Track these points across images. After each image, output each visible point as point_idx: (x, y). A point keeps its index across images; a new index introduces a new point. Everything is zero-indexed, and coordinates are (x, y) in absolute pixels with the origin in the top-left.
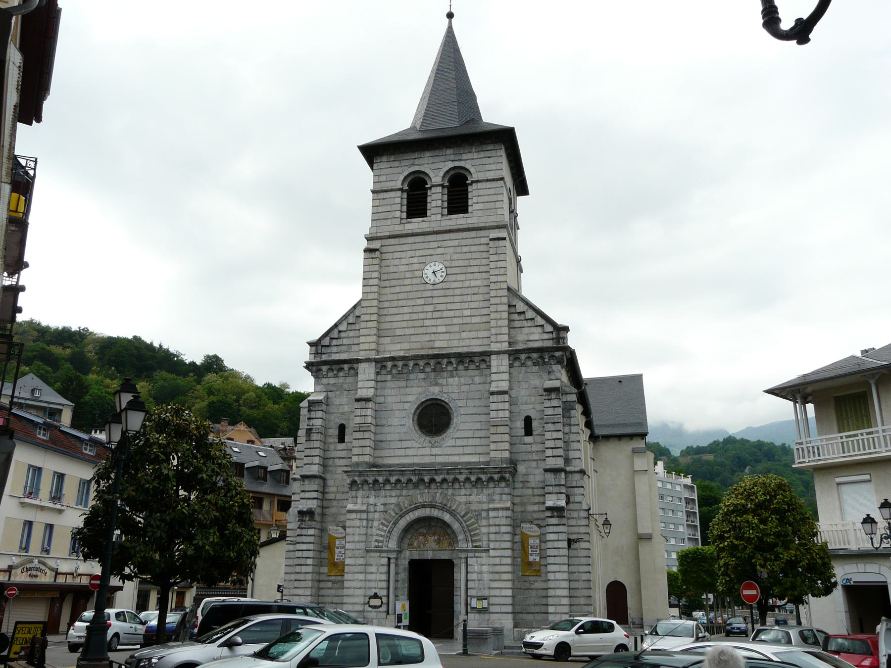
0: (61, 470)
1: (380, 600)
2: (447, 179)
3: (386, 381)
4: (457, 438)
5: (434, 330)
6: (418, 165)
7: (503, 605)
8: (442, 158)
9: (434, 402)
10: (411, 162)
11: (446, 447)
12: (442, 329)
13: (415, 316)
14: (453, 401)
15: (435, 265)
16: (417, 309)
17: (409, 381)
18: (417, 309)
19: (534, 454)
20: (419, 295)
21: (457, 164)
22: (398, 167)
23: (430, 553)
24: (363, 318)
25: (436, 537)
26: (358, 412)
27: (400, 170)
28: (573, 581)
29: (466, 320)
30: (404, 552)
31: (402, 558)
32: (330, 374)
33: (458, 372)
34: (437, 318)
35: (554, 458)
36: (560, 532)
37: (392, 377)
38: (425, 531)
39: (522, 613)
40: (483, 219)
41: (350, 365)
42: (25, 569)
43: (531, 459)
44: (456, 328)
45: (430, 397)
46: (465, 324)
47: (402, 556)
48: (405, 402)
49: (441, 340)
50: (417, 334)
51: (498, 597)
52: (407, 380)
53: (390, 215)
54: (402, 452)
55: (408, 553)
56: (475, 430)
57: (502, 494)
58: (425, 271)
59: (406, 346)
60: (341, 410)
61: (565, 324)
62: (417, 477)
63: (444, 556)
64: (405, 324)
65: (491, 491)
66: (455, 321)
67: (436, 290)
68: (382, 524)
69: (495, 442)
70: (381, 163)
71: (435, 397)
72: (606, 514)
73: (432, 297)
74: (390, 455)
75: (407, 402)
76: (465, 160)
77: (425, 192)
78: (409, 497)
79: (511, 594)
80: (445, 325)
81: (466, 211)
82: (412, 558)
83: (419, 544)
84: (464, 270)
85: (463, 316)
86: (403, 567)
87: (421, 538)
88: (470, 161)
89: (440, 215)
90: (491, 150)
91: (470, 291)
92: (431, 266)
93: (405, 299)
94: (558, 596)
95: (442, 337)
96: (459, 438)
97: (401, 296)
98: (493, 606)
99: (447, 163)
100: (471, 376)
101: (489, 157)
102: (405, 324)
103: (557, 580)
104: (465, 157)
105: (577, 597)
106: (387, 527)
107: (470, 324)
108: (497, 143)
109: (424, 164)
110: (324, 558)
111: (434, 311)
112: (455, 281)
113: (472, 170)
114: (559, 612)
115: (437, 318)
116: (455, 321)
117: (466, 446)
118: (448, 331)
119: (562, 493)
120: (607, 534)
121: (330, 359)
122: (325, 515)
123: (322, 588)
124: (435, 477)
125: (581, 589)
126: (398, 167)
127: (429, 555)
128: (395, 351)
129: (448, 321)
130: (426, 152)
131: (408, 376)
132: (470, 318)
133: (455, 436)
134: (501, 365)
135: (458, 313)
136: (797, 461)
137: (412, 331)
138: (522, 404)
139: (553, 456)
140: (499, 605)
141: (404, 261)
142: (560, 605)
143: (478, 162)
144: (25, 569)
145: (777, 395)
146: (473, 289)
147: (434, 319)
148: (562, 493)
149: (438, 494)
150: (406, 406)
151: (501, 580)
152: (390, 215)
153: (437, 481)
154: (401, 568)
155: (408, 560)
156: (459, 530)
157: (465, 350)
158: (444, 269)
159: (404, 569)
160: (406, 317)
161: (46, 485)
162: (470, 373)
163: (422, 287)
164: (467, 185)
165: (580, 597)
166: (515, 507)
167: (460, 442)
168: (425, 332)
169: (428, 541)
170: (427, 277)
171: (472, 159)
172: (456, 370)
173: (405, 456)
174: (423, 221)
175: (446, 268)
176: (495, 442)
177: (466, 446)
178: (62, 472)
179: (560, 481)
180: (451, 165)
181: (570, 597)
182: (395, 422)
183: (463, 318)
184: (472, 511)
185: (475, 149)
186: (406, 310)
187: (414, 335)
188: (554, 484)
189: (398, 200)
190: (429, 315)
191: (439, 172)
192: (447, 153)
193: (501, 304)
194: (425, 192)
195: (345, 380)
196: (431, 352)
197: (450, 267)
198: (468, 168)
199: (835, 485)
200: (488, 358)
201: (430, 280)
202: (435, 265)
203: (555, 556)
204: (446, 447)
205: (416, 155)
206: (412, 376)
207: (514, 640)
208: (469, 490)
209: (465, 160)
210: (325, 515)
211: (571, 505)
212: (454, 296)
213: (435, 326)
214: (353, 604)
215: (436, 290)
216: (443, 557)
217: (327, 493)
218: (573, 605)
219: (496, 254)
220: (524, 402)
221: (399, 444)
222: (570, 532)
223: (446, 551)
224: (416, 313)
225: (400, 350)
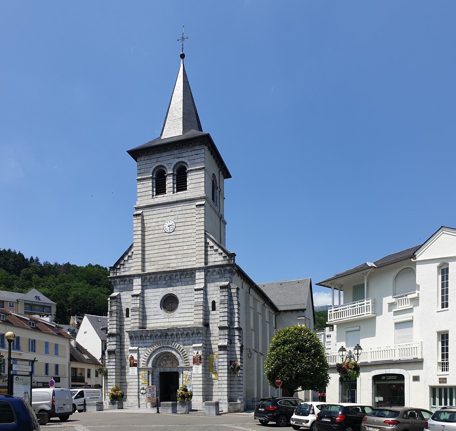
1: (145, 391)
2: (155, 174)
3: (147, 285)
4: (180, 313)
5: (170, 257)
7: (198, 392)
9: (171, 295)
10: (156, 160)
13: (160, 251)
14: (179, 294)
16: (161, 247)
17: (158, 285)
18: (161, 247)
20: (162, 239)
21: (180, 160)
23: (168, 369)
24: (135, 253)
26: (133, 302)
27: (148, 166)
29: (185, 252)
30: (157, 368)
31: (156, 371)
32: (121, 283)
33: (181, 279)
34: (171, 251)
35: (223, 322)
36: (224, 358)
37: (150, 283)
39: (209, 395)
42: (4, 380)
43: (215, 322)
44: (180, 256)
45: (168, 293)
46: (185, 254)
47: (156, 370)
49: (173, 263)
50: (162, 260)
51: (197, 388)
52: (157, 284)
54: (155, 321)
55: (158, 369)
56: (189, 309)
58: (165, 226)
60: (127, 301)
61: (68, 262)
62: (175, 332)
64: (155, 255)
65: (194, 338)
66: (180, 252)
68: (145, 356)
69: (196, 314)
71: (170, 293)
72: (250, 349)
73: (168, 240)
74: (150, 323)
76: (184, 157)
77: (165, 178)
78: (157, 343)
80: (175, 255)
81: (186, 189)
82: (160, 371)
83: (163, 364)
85: (184, 250)
86: (157, 375)
87: (164, 362)
88: (187, 157)
89: (172, 192)
91: (187, 236)
92: (167, 223)
95: (173, 261)
96: (182, 313)
97: (153, 240)
99: (175, 159)
100: (187, 281)
101: (197, 154)
102: (155, 255)
103: (223, 380)
104: (184, 155)
105: (234, 388)
106: (147, 357)
107: (187, 253)
108: (201, 144)
109: (163, 161)
110: (122, 372)
112: (179, 231)
115: (171, 251)
120: (250, 358)
121: (121, 275)
123: (122, 386)
124: (168, 333)
125: (236, 384)
127: (168, 370)
130: (164, 153)
133: (180, 312)
134: (201, 275)
135: (181, 248)
136: (329, 320)
137: (159, 259)
139: (223, 321)
142: (224, 392)
143: (191, 158)
144: (4, 380)
145: (318, 285)
147: (170, 252)
148: (226, 339)
153: (169, 335)
154: (155, 376)
155: (159, 372)
157: (185, 268)
158: (174, 224)
159: (157, 377)
160: (156, 251)
162: (187, 279)
163: (163, 235)
164: (165, 177)
165: (235, 388)
167: (182, 315)
169: (167, 363)
170: (166, 229)
171: (188, 156)
173: (157, 323)
174: (163, 196)
175: (175, 223)
176: (196, 314)
178: (19, 336)
180: (177, 160)
181: (230, 388)
184: (185, 348)
186: (156, 247)
187: (160, 261)
188: (222, 334)
189: (151, 184)
190: (167, 250)
192: (175, 153)
194: (165, 178)
195: (128, 286)
198: (186, 162)
199: (345, 333)
200: (195, 271)
201: (167, 230)
202: (169, 222)
203: (222, 369)
205: (159, 155)
207: (203, 408)
209: (184, 157)
211: (232, 344)
212: (179, 239)
213: (170, 255)
214: (133, 392)
216: (174, 371)
219: (199, 214)
220: (212, 294)
221: (154, 317)
222: (231, 358)
224: (161, 249)
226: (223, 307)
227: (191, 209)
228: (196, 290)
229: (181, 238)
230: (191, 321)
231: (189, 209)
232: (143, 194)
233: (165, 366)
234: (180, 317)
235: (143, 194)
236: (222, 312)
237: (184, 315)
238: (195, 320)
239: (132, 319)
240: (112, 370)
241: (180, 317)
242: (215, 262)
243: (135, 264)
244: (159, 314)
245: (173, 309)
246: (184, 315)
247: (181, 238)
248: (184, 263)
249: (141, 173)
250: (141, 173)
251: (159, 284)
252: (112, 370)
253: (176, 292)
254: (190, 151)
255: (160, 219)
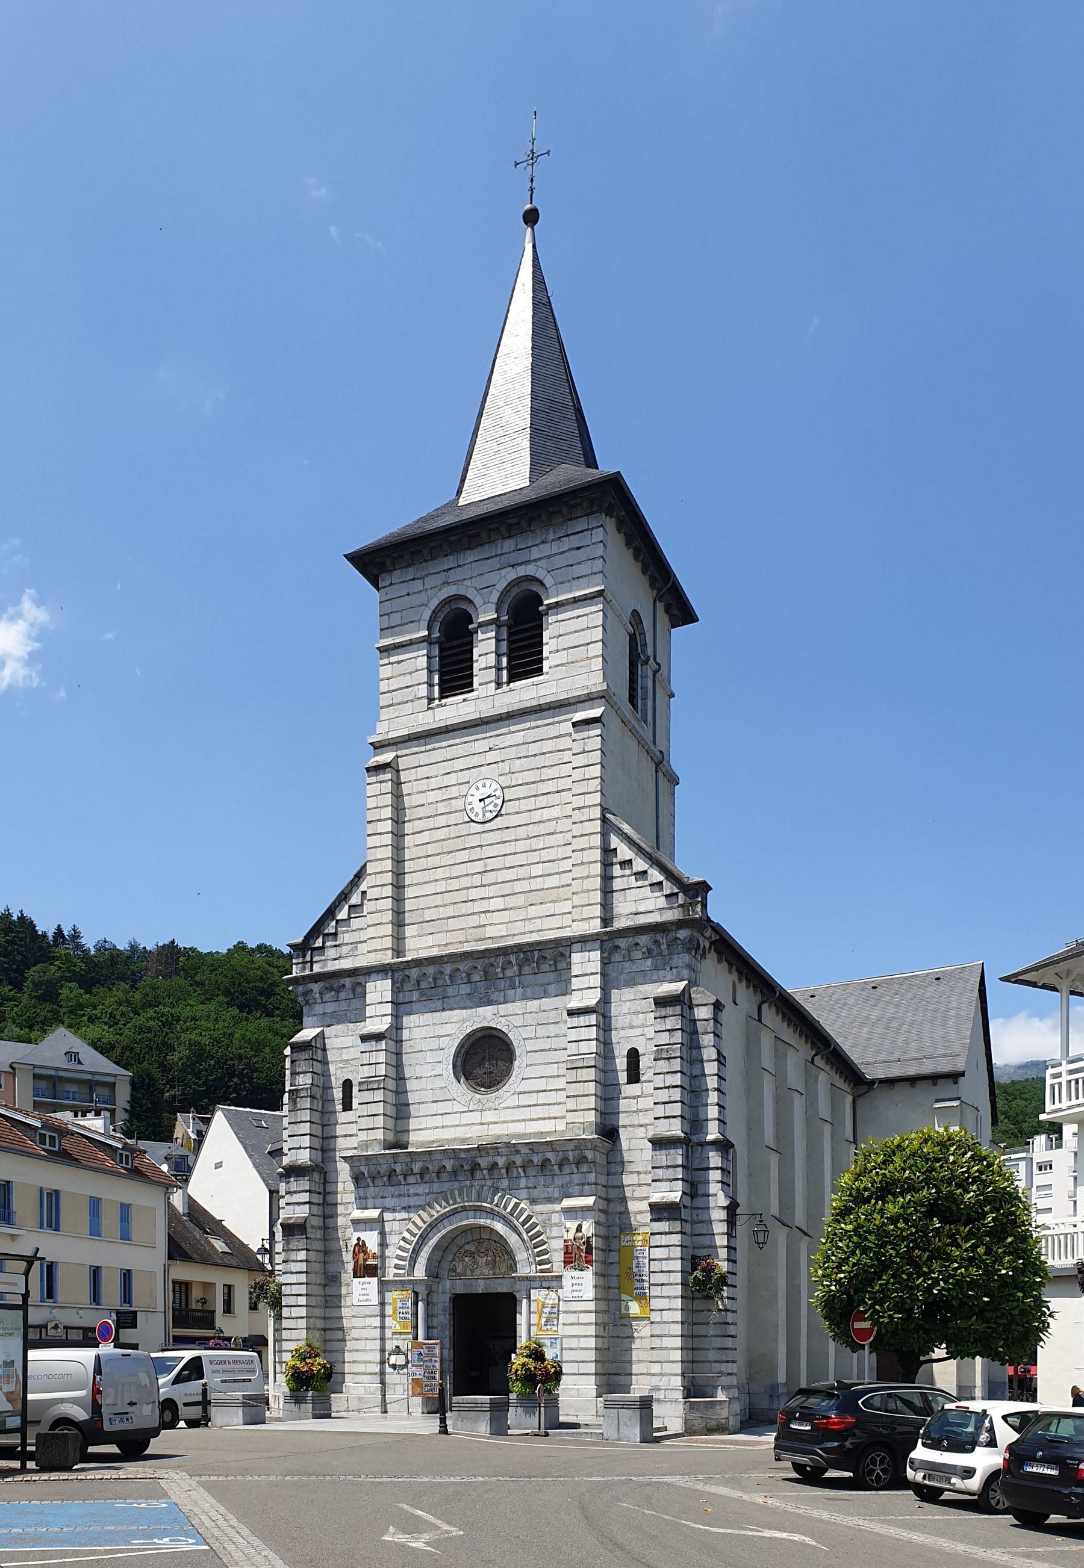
0: (51, 1185)
3: (412, 1002)
6: (455, 583)
8: (494, 563)
11: (504, 1108)
12: (497, 904)
13: (455, 884)
14: (515, 1029)
15: (484, 786)
19: (641, 1114)
21: (522, 571)
22: (420, 592)
25: (489, 1258)
28: (699, 1324)
32: (328, 996)
33: (522, 978)
34: (490, 885)
35: (667, 1120)
37: (421, 995)
38: (473, 1249)
40: (566, 684)
41: (353, 979)
44: (520, 900)
45: (480, 1026)
47: (440, 1288)
48: (441, 1037)
50: (459, 916)
53: (409, 694)
54: (438, 1121)
55: (448, 1284)
57: (583, 1184)
59: (443, 939)
63: (502, 1287)
64: (438, 900)
65: (567, 1179)
66: (518, 887)
67: (488, 831)
68: (404, 1239)
70: (393, 587)
71: (486, 1025)
73: (481, 846)
75: (445, 1036)
76: (536, 560)
79: (283, 1321)
80: (502, 896)
82: (454, 1292)
83: (465, 1267)
84: (532, 790)
90: (582, 531)
92: (478, 789)
93: (438, 854)
94: (666, 1349)
95: (497, 917)
96: (525, 1093)
97: (431, 849)
98: (287, 1342)
99: (503, 572)
100: (542, 985)
102: (438, 900)
104: (535, 553)
105: (704, 1349)
107: (543, 889)
109: (465, 579)
111: (484, 872)
112: (517, 813)
113: (548, 581)
114: (668, 1372)
115: (490, 885)
116: (518, 887)
117: (535, 1105)
118: (507, 907)
119: (678, 1179)
122: (329, 1228)
123: (330, 1340)
124: (479, 1160)
126: (420, 592)
127: (480, 1287)
128: (424, 948)
129: (506, 889)
131: (445, 991)
132: (541, 878)
133: (518, 1090)
135: (522, 872)
137: (450, 911)
138: (623, 1029)
139: (666, 1117)
140: (577, 1362)
141: (434, 783)
143: (559, 561)
146: (547, 824)
147: (484, 886)
149: (485, 1188)
150: (443, 1043)
151: (579, 1324)
152: (409, 694)
154: (438, 1309)
156: (518, 1245)
157: (535, 938)
159: (444, 1310)
161: (110, 1220)
163: (464, 829)
165: (709, 1349)
166: (611, 1205)
167: (525, 1100)
168: (469, 912)
169: (477, 1264)
171: (549, 557)
172: (520, 975)
173: (443, 1127)
174: (464, 700)
176: (574, 1096)
177: (535, 1105)
179: (675, 1159)
180: (511, 575)
182: (425, 1070)
183: (531, 881)
185: (554, 532)
186: (440, 873)
188: (664, 1164)
189: (423, 662)
191: (492, 591)
193: (590, 848)
195: (349, 1006)
196: (481, 946)
197: (509, 787)
201: (477, 815)
202: (484, 786)
203: (662, 1285)
204: (504, 1108)
205: (450, 562)
206: (450, 991)
207: (597, 1416)
208: (532, 1179)
209: (536, 560)
210: (329, 1228)
215: (488, 831)
216: (500, 1290)
217: (329, 1193)
218: (696, 1362)
219: (584, 752)
221: (434, 1108)
223: (504, 1280)
225: (433, 947)
226: (667, 1070)
227: (558, 737)
228: (571, 1013)
229: (521, 839)
230: (555, 1118)
231: (549, 739)
232: (397, 697)
233: (469, 1272)
234: (519, 1107)
235: (397, 697)
236: (661, 1088)
237: (533, 1099)
238: (571, 1117)
239: (363, 1116)
240: (296, 1290)
241: (519, 1107)
242: (636, 914)
243: (371, 932)
244: (451, 1098)
245: (496, 1080)
246: (533, 1099)
247: (521, 839)
248: (533, 921)
249: (392, 627)
250: (392, 627)
251: (449, 997)
252: (296, 1290)
253: (507, 1023)
254: (554, 540)
255: (453, 779)
